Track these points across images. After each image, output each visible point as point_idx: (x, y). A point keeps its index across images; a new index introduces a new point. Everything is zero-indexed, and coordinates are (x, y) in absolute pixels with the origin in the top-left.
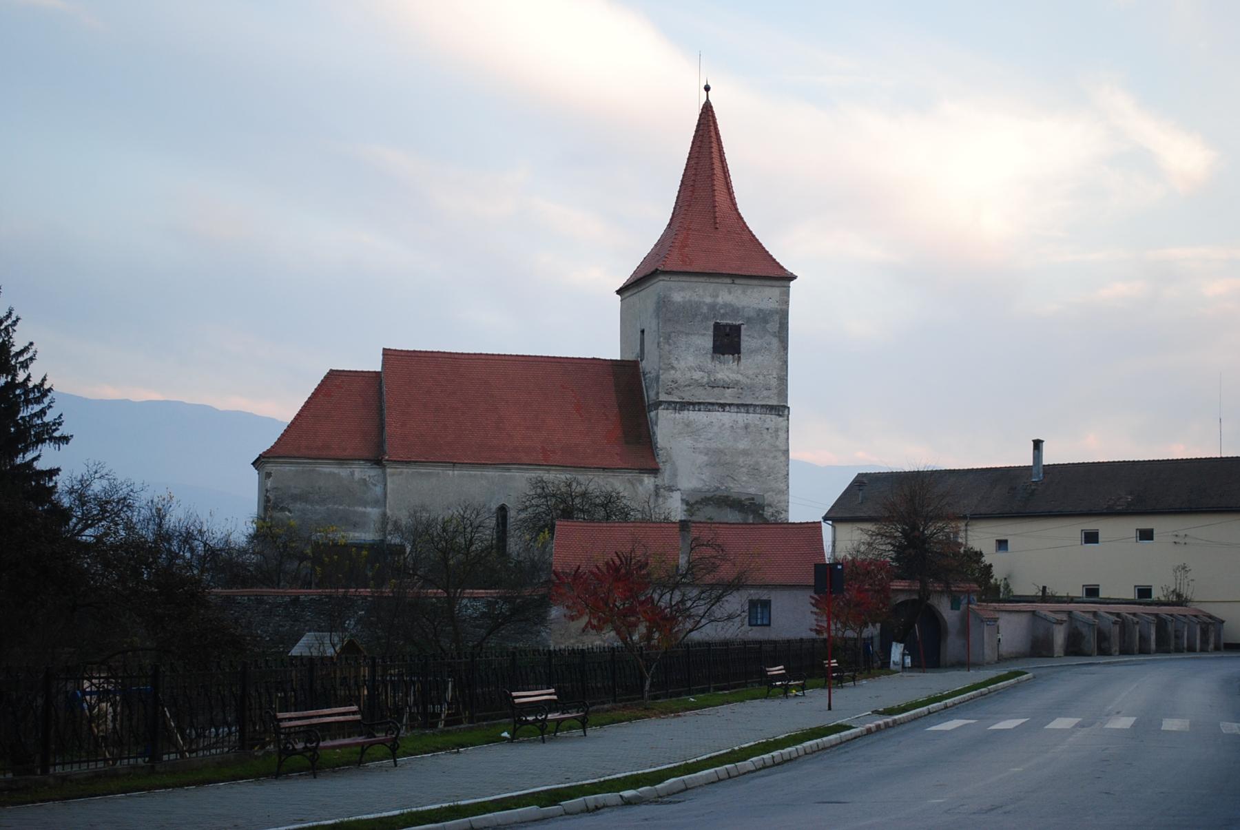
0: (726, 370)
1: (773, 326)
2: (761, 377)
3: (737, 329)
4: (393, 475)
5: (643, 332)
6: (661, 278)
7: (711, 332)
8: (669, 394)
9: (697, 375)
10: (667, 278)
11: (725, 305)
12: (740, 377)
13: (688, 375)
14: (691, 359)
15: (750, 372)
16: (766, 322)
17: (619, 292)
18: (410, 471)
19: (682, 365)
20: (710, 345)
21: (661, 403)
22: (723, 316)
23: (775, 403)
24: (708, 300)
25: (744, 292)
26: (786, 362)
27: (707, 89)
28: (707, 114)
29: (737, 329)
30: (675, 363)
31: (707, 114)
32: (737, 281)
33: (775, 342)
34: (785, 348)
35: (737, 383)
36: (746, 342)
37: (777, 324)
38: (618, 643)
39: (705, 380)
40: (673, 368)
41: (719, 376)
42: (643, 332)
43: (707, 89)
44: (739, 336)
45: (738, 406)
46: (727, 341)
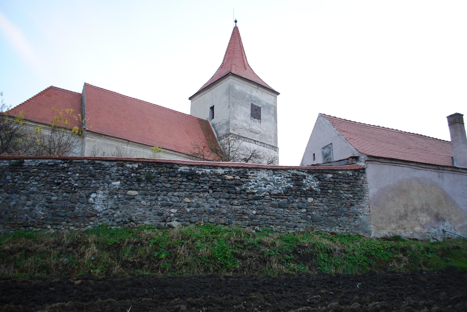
0: (255, 125)
1: (272, 111)
2: (268, 132)
3: (260, 108)
4: (89, 141)
5: (212, 108)
6: (231, 77)
7: (250, 107)
8: (234, 130)
9: (245, 125)
10: (233, 78)
11: (255, 97)
12: (261, 130)
13: (241, 124)
14: (242, 117)
15: (264, 129)
16: (270, 109)
17: (190, 98)
18: (101, 141)
19: (239, 118)
20: (250, 112)
21: (230, 134)
22: (255, 101)
23: (274, 145)
24: (249, 93)
25: (262, 94)
26: (277, 128)
27: (236, 22)
28: (236, 33)
29: (260, 108)
30: (236, 117)
31: (236, 33)
32: (259, 88)
33: (273, 118)
34: (277, 122)
35: (260, 132)
36: (263, 115)
37: (273, 110)
38: (406, 264)
39: (248, 128)
40: (235, 118)
41: (253, 127)
42: (212, 108)
43: (236, 22)
44: (260, 110)
45: (261, 143)
46: (256, 113)
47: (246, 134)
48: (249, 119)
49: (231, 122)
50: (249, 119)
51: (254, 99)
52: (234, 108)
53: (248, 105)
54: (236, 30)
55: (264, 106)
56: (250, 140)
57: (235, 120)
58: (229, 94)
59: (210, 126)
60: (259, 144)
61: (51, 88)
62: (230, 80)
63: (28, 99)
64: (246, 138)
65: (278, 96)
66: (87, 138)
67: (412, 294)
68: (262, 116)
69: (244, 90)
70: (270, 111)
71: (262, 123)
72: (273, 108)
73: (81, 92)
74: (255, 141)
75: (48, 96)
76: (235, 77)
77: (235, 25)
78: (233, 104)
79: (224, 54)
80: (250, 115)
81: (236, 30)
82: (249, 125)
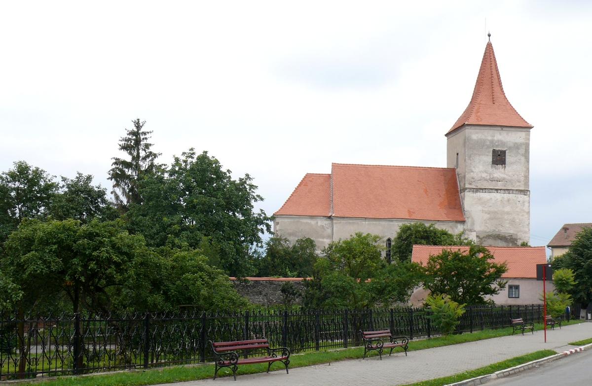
0: (499, 172)
1: (522, 151)
4: (336, 223)
6: (467, 127)
7: (491, 154)
8: (471, 184)
9: (484, 175)
11: (498, 141)
12: (505, 176)
14: (481, 167)
15: (510, 174)
17: (446, 135)
22: (497, 146)
24: (490, 138)
25: (507, 134)
27: (489, 35)
28: (489, 56)
29: (504, 152)
33: (523, 159)
35: (504, 179)
39: (488, 177)
41: (495, 175)
43: (489, 35)
45: (504, 190)
46: (499, 158)
47: (486, 185)
48: (490, 169)
49: (467, 176)
50: (490, 168)
51: (497, 144)
52: (471, 160)
53: (489, 152)
54: (489, 47)
55: (510, 148)
56: (491, 191)
57: (472, 173)
58: (465, 146)
59: (455, 174)
60: (502, 192)
61: (308, 176)
62: (468, 131)
63: (291, 193)
64: (485, 189)
65: (531, 130)
66: (334, 221)
67: (37, 323)
68: (507, 160)
69: (483, 137)
70: (519, 151)
71: (507, 168)
72: (524, 147)
73: (330, 173)
74: (497, 190)
75: (305, 185)
76: (473, 128)
77: (488, 41)
78: (470, 157)
79: (497, 62)
80: (491, 163)
81: (489, 47)
82: (490, 174)
